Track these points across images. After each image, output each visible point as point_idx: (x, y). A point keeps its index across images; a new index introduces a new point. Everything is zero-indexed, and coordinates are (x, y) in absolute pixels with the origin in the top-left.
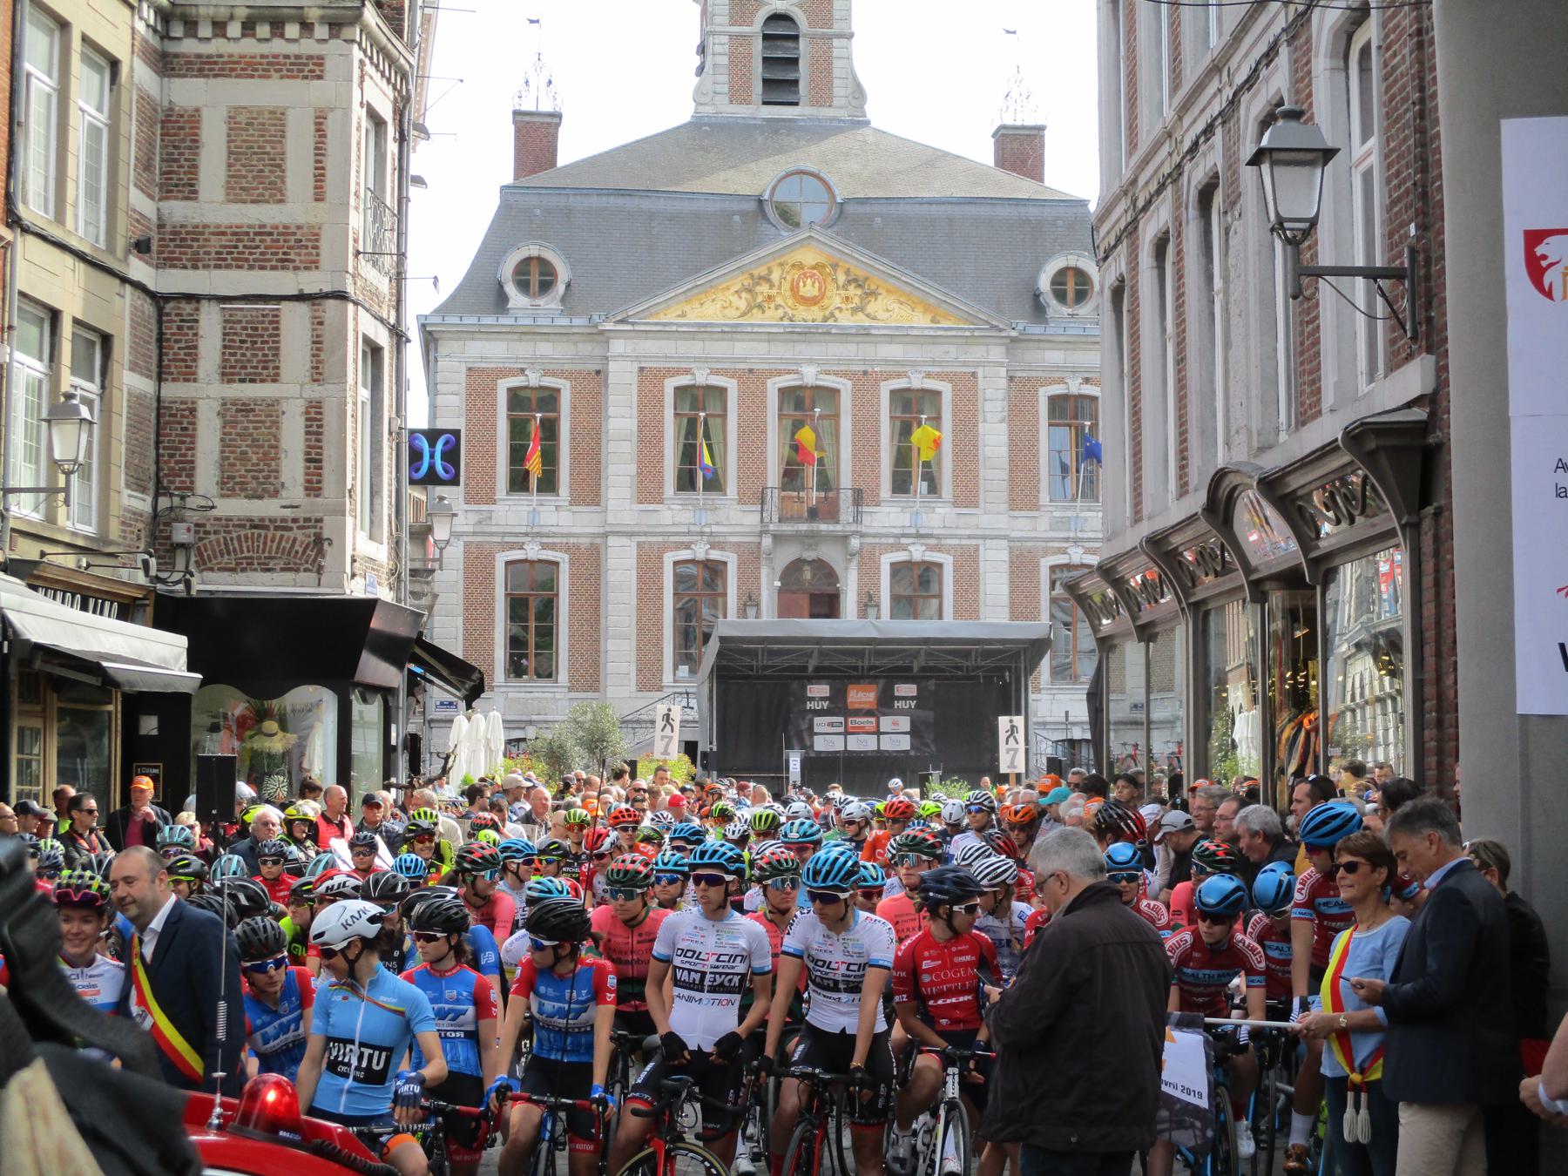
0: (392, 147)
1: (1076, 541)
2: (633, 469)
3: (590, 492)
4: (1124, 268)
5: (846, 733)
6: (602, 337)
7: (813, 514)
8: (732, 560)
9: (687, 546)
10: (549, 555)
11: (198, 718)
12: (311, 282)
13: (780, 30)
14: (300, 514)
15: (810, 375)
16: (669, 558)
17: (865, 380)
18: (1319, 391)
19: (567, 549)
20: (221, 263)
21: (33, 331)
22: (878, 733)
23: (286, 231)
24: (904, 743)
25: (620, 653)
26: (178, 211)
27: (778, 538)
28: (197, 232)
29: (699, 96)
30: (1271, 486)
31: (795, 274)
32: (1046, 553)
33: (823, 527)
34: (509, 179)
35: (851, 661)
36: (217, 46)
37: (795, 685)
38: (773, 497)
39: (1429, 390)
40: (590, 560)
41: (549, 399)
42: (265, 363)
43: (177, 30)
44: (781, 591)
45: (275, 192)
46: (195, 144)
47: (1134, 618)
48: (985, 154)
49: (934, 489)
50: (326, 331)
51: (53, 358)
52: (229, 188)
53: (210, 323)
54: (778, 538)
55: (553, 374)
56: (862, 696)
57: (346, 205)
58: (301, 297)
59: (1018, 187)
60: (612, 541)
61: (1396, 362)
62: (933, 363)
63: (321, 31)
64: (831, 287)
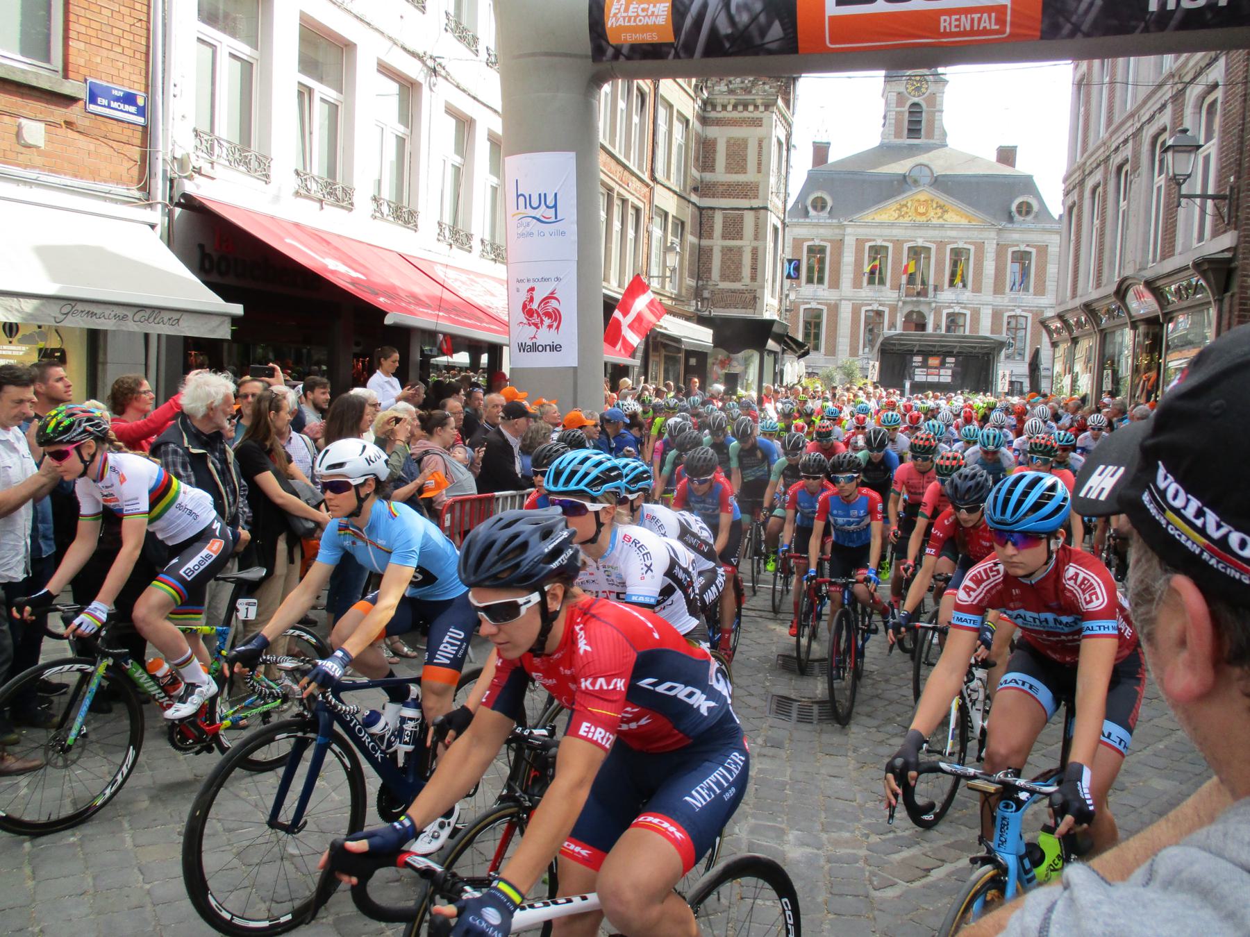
0: (784, 153)
1: (1019, 307)
2: (852, 276)
3: (835, 284)
4: (1076, 198)
5: (927, 375)
6: (843, 227)
7: (919, 294)
8: (887, 310)
9: (870, 305)
10: (820, 307)
11: (710, 361)
12: (755, 203)
13: (915, 109)
14: (749, 288)
15: (920, 242)
16: (864, 309)
17: (941, 245)
18: (1174, 246)
19: (826, 304)
20: (723, 196)
21: (659, 219)
22: (939, 375)
23: (747, 184)
24: (949, 379)
25: (844, 343)
26: (708, 176)
27: (904, 303)
28: (715, 184)
29: (883, 134)
30: (1151, 285)
31: (916, 204)
32: (1007, 311)
33: (922, 299)
34: (810, 167)
35: (931, 349)
36: (723, 114)
37: (908, 357)
38: (903, 287)
39: (1233, 245)
40: (834, 309)
41: (822, 250)
42: (738, 233)
43: (709, 108)
44: (904, 322)
45: (743, 170)
46: (715, 151)
47: (1070, 334)
48: (993, 157)
49: (964, 286)
50: (760, 221)
51: (665, 229)
52: (726, 168)
53: (718, 219)
54: (904, 303)
55: (825, 240)
56: (933, 361)
57: (768, 174)
58: (752, 209)
59: (1005, 170)
60: (843, 302)
61: (1216, 233)
62: (968, 238)
63: (762, 108)
64: (930, 209)
